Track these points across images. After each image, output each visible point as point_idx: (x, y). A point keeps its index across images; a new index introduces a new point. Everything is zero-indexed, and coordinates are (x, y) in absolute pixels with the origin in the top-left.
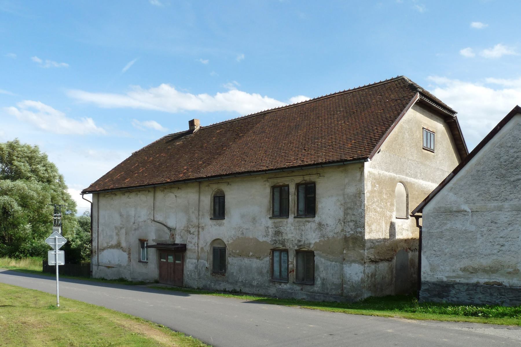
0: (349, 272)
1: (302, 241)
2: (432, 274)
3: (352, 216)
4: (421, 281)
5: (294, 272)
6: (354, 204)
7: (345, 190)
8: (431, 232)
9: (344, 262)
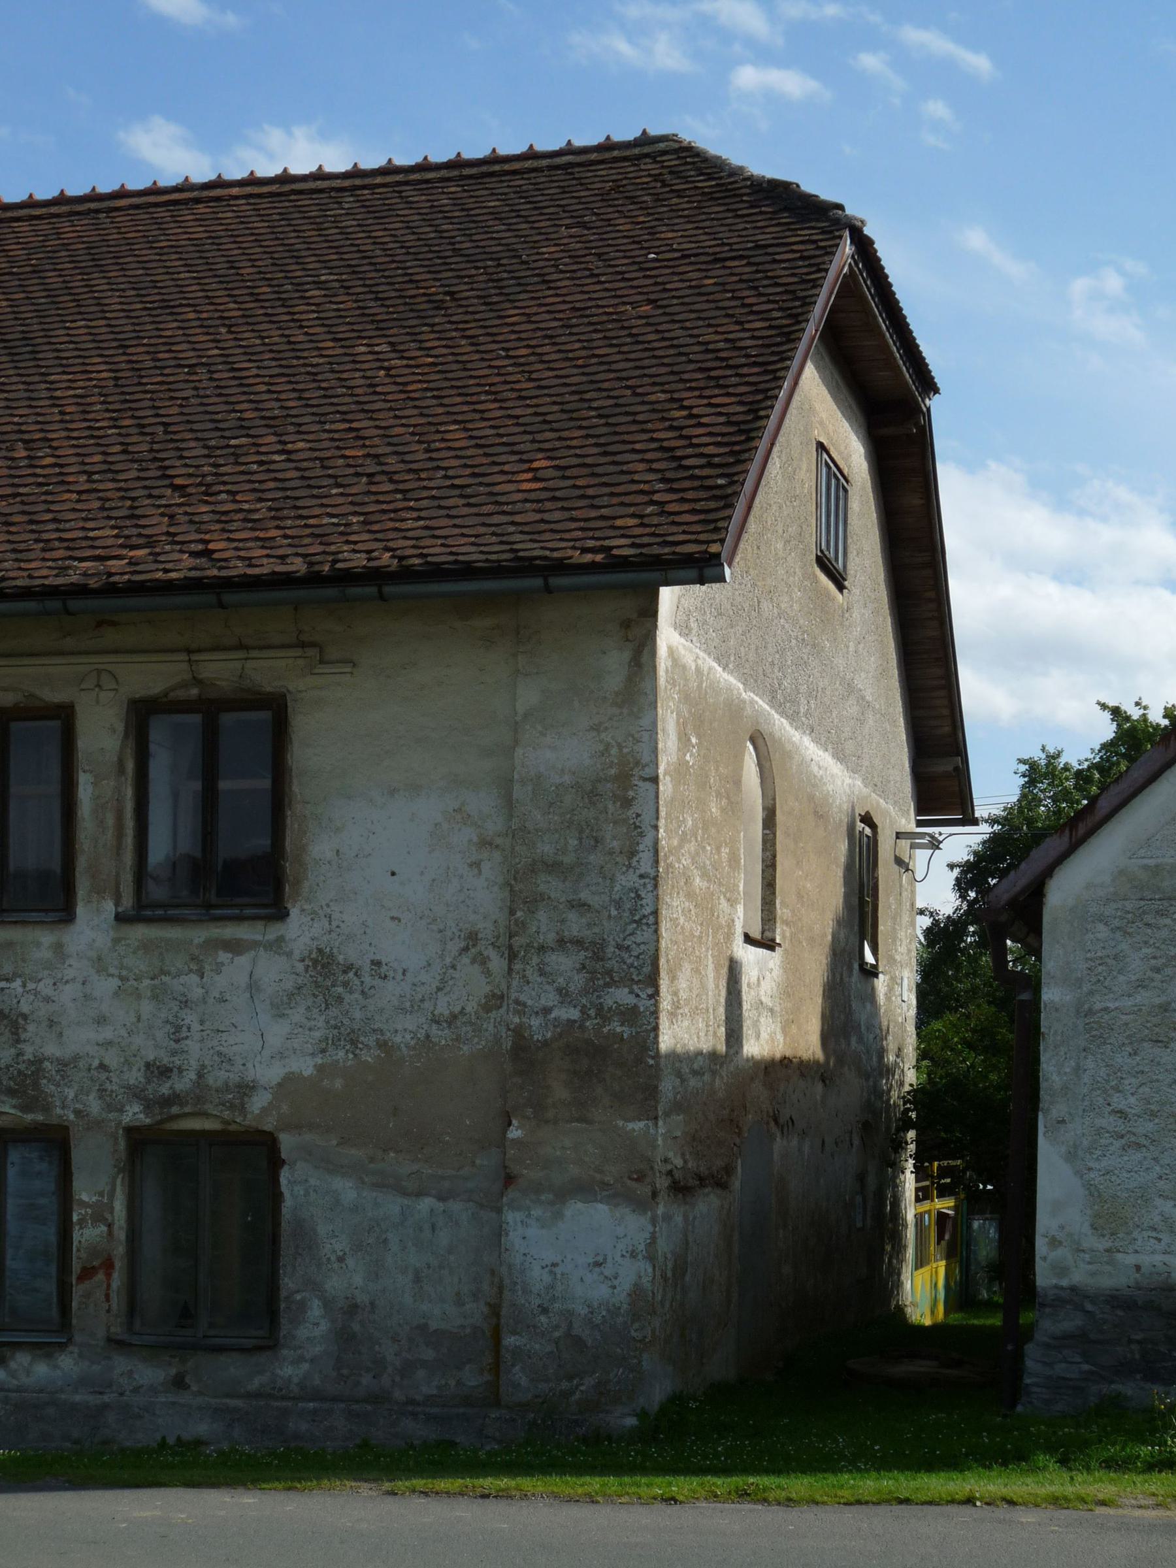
0: (549, 1256)
1: (180, 1070)
2: (1101, 1244)
3: (572, 916)
4: (1039, 1289)
5: (116, 1275)
6: (580, 839)
7: (519, 752)
8: (1098, 1006)
9: (512, 1193)
